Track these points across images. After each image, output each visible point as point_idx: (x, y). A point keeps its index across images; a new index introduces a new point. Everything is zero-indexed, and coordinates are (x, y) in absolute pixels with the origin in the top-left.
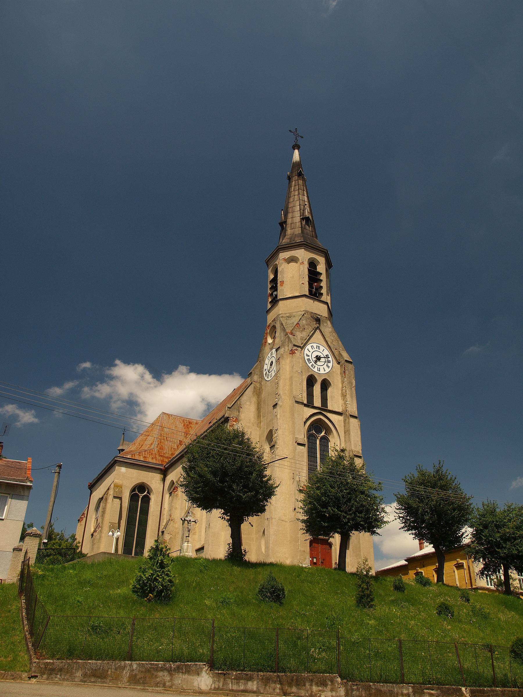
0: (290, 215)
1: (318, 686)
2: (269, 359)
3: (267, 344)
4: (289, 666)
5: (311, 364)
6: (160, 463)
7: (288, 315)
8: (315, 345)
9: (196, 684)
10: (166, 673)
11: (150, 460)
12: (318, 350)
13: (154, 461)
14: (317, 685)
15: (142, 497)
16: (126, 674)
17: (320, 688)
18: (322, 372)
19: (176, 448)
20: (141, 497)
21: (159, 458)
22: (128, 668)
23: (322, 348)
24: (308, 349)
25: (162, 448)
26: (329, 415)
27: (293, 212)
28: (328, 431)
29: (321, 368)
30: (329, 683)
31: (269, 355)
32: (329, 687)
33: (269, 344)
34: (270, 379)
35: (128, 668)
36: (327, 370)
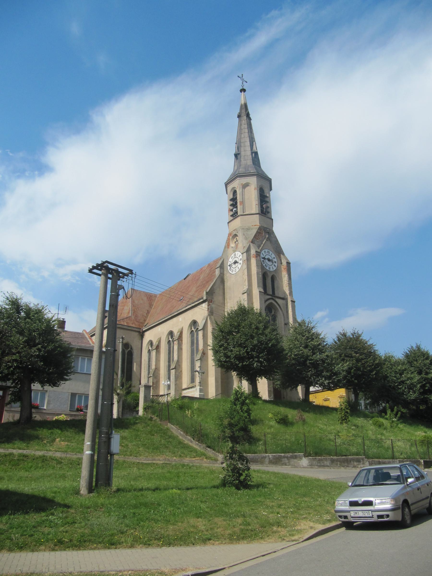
0: (242, 149)
1: (357, 462)
2: (233, 258)
3: (230, 247)
4: (198, 463)
5: (265, 264)
6: (138, 327)
7: (247, 227)
8: (266, 250)
9: (301, 464)
10: (286, 459)
11: (131, 325)
12: (268, 254)
13: (134, 326)
14: (356, 462)
15: (127, 353)
16: (267, 460)
17: (358, 463)
18: (271, 270)
19: (146, 315)
20: (127, 351)
21: (137, 323)
22: (267, 457)
23: (271, 252)
24: (262, 254)
25: (136, 316)
26: (277, 300)
27: (245, 146)
28: (276, 309)
29: (271, 267)
30: (362, 461)
31: (233, 255)
32: (362, 463)
33: (232, 247)
34: (234, 273)
35: (267, 457)
36: (275, 268)
